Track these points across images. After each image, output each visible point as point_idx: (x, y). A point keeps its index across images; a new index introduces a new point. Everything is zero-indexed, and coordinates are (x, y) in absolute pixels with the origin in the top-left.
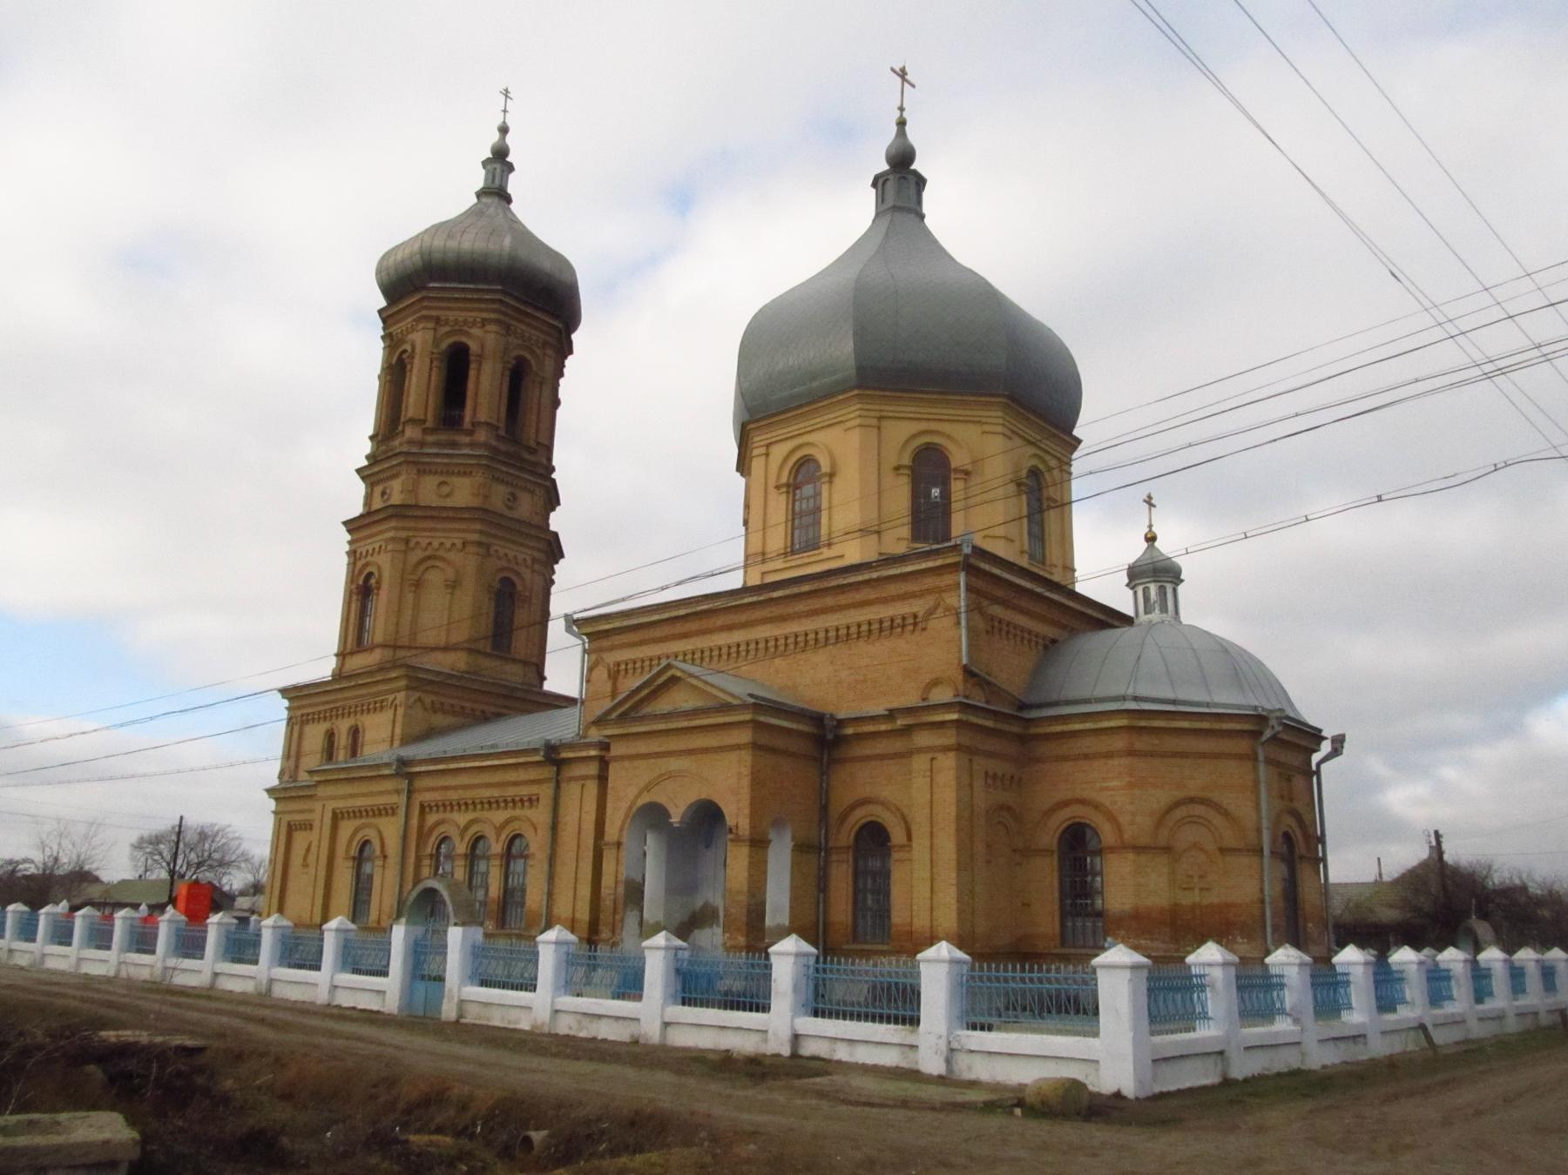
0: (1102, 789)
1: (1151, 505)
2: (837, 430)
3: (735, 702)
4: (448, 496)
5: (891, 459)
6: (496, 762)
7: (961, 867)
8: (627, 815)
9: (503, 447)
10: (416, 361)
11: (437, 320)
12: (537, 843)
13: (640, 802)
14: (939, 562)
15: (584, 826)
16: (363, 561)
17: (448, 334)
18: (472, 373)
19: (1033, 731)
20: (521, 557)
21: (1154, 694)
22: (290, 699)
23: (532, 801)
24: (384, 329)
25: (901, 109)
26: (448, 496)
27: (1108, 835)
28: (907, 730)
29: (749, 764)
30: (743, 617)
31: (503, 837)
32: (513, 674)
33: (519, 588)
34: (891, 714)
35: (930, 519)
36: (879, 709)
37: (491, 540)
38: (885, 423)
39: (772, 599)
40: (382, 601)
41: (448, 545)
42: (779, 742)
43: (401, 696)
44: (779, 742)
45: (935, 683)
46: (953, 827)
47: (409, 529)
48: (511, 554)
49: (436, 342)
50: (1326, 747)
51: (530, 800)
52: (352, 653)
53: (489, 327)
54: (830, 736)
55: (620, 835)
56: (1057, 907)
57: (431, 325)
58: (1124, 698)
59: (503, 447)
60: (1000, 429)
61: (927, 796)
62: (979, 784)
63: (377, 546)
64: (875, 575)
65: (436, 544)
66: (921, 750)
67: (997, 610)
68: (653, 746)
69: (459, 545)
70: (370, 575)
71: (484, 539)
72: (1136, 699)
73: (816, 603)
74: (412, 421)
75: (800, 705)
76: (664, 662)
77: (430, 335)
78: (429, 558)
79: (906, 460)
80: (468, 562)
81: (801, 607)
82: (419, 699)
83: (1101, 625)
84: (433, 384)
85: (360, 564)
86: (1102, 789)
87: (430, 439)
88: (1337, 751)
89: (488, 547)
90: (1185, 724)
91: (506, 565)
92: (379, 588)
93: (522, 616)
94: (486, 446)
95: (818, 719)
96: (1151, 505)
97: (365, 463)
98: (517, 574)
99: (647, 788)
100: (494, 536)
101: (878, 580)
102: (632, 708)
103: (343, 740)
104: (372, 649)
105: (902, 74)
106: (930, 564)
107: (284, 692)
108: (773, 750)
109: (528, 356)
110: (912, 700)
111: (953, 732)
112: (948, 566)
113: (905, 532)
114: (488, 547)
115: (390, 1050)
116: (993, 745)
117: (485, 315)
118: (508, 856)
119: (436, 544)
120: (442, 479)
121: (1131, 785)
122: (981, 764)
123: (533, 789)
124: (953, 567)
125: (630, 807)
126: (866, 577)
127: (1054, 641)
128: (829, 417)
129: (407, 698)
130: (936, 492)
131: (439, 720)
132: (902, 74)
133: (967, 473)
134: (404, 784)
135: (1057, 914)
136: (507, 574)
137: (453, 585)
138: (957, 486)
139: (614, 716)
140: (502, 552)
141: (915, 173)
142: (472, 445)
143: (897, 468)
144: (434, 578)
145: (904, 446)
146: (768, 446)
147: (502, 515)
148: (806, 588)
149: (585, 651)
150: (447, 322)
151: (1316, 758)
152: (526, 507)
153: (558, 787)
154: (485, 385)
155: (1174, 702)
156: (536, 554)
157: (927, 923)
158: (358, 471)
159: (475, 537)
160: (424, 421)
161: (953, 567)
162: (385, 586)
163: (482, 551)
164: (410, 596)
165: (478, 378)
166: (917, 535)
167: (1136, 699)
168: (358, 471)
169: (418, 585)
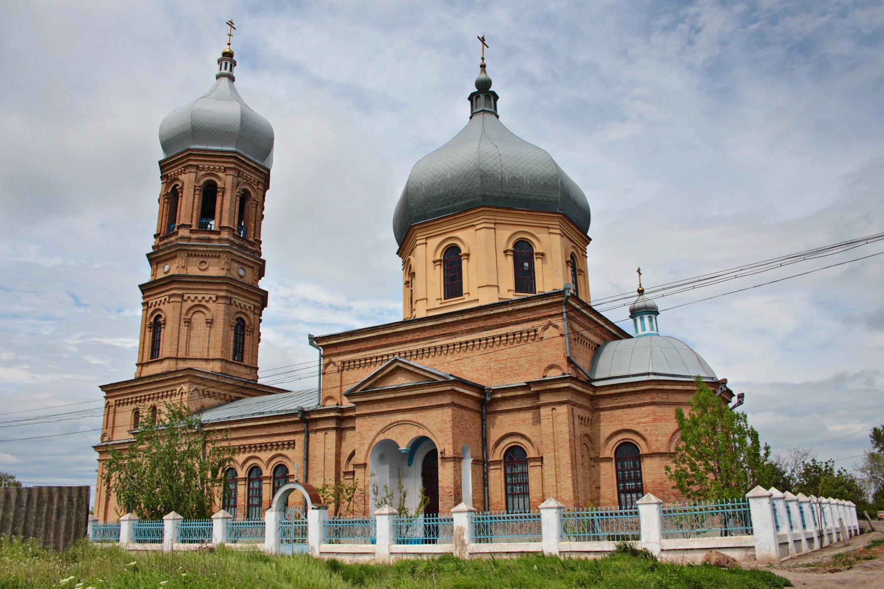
0: (639, 423)
1: (640, 274)
2: (472, 230)
3: (440, 380)
4: (204, 270)
5: (502, 247)
6: (266, 422)
7: (574, 467)
8: (369, 448)
9: (237, 241)
10: (185, 191)
11: (197, 167)
12: (295, 469)
13: (377, 440)
14: (549, 301)
15: (328, 457)
16: (153, 308)
17: (205, 175)
18: (219, 199)
19: (598, 393)
20: (248, 306)
21: (632, 373)
22: (107, 392)
23: (291, 445)
24: (162, 173)
25: (483, 59)
26: (204, 270)
27: (644, 449)
28: (537, 395)
29: (450, 414)
30: (426, 334)
31: (270, 466)
32: (242, 373)
33: (247, 323)
34: (529, 385)
35: (524, 278)
36: (522, 383)
37: (233, 296)
38: (497, 226)
39: (445, 323)
40: (167, 334)
41: (207, 298)
42: (464, 402)
43: (185, 388)
44: (464, 402)
45: (552, 367)
46: (568, 445)
47: (183, 289)
48: (243, 304)
49: (197, 180)
50: (735, 400)
51: (289, 444)
52: (148, 363)
53: (229, 172)
54: (488, 399)
55: (366, 459)
56: (616, 488)
57: (194, 170)
58: (648, 374)
59: (237, 241)
60: (558, 231)
61: (550, 431)
62: (577, 422)
63: (163, 299)
64: (510, 309)
65: (200, 297)
66: (545, 405)
67: (577, 327)
68: (384, 408)
69: (214, 299)
70: (159, 316)
71: (229, 295)
72: (655, 374)
73: (474, 325)
74: (183, 226)
75: (474, 381)
76: (392, 358)
77: (193, 175)
78: (241, 312)
79: (510, 247)
80: (218, 310)
81: (463, 327)
82: (196, 389)
83: (617, 338)
84: (196, 204)
85: (151, 311)
86: (639, 423)
87: (194, 236)
88: (740, 403)
89: (230, 299)
90: (680, 387)
91: (239, 309)
92: (165, 324)
93: (248, 339)
94: (228, 240)
95: (480, 389)
96: (640, 274)
97: (152, 251)
98: (246, 315)
99: (383, 431)
100: (234, 293)
101: (533, 307)
102: (371, 386)
103: (145, 413)
104: (162, 360)
105: (483, 40)
106: (545, 302)
107: (103, 387)
108: (461, 407)
109: (250, 190)
110: (537, 377)
111: (335, 421)
112: (556, 303)
113: (512, 286)
114: (230, 299)
115: (505, 557)
116: (581, 401)
117: (225, 165)
118: (249, 479)
119: (200, 297)
120: (202, 259)
121: (655, 420)
122: (578, 412)
123: (291, 438)
124: (559, 304)
125: (371, 444)
126: (505, 310)
127: (598, 346)
128: (464, 223)
129: (190, 388)
130: (526, 264)
131: (208, 401)
132: (483, 40)
133: (543, 254)
134: (305, 425)
135: (616, 491)
136: (238, 316)
137: (210, 323)
138: (538, 263)
139: (358, 391)
140: (238, 302)
141: (493, 93)
142: (220, 240)
143: (505, 252)
144: (199, 319)
145: (437, 250)
146: (427, 238)
147: (237, 281)
148: (467, 317)
149: (321, 356)
150: (203, 169)
151: (730, 405)
152: (248, 275)
153: (308, 437)
154: (226, 205)
155: (674, 376)
156: (256, 304)
157: (170, 548)
158: (148, 255)
159: (223, 294)
160: (191, 226)
161: (559, 304)
162: (169, 323)
163: (228, 302)
164: (184, 329)
165: (222, 201)
166: (518, 288)
167: (655, 374)
168: (148, 255)
169: (189, 322)
